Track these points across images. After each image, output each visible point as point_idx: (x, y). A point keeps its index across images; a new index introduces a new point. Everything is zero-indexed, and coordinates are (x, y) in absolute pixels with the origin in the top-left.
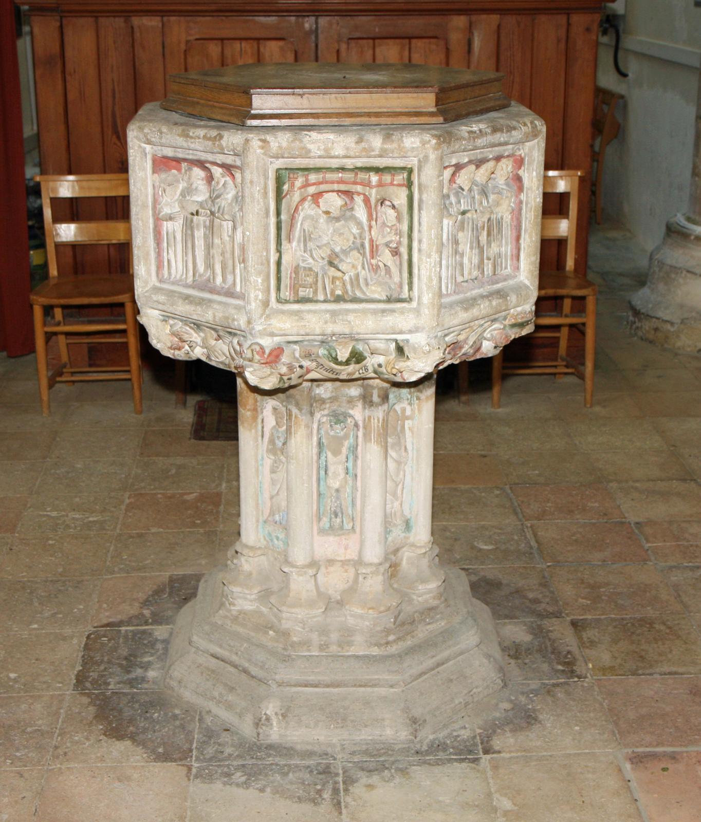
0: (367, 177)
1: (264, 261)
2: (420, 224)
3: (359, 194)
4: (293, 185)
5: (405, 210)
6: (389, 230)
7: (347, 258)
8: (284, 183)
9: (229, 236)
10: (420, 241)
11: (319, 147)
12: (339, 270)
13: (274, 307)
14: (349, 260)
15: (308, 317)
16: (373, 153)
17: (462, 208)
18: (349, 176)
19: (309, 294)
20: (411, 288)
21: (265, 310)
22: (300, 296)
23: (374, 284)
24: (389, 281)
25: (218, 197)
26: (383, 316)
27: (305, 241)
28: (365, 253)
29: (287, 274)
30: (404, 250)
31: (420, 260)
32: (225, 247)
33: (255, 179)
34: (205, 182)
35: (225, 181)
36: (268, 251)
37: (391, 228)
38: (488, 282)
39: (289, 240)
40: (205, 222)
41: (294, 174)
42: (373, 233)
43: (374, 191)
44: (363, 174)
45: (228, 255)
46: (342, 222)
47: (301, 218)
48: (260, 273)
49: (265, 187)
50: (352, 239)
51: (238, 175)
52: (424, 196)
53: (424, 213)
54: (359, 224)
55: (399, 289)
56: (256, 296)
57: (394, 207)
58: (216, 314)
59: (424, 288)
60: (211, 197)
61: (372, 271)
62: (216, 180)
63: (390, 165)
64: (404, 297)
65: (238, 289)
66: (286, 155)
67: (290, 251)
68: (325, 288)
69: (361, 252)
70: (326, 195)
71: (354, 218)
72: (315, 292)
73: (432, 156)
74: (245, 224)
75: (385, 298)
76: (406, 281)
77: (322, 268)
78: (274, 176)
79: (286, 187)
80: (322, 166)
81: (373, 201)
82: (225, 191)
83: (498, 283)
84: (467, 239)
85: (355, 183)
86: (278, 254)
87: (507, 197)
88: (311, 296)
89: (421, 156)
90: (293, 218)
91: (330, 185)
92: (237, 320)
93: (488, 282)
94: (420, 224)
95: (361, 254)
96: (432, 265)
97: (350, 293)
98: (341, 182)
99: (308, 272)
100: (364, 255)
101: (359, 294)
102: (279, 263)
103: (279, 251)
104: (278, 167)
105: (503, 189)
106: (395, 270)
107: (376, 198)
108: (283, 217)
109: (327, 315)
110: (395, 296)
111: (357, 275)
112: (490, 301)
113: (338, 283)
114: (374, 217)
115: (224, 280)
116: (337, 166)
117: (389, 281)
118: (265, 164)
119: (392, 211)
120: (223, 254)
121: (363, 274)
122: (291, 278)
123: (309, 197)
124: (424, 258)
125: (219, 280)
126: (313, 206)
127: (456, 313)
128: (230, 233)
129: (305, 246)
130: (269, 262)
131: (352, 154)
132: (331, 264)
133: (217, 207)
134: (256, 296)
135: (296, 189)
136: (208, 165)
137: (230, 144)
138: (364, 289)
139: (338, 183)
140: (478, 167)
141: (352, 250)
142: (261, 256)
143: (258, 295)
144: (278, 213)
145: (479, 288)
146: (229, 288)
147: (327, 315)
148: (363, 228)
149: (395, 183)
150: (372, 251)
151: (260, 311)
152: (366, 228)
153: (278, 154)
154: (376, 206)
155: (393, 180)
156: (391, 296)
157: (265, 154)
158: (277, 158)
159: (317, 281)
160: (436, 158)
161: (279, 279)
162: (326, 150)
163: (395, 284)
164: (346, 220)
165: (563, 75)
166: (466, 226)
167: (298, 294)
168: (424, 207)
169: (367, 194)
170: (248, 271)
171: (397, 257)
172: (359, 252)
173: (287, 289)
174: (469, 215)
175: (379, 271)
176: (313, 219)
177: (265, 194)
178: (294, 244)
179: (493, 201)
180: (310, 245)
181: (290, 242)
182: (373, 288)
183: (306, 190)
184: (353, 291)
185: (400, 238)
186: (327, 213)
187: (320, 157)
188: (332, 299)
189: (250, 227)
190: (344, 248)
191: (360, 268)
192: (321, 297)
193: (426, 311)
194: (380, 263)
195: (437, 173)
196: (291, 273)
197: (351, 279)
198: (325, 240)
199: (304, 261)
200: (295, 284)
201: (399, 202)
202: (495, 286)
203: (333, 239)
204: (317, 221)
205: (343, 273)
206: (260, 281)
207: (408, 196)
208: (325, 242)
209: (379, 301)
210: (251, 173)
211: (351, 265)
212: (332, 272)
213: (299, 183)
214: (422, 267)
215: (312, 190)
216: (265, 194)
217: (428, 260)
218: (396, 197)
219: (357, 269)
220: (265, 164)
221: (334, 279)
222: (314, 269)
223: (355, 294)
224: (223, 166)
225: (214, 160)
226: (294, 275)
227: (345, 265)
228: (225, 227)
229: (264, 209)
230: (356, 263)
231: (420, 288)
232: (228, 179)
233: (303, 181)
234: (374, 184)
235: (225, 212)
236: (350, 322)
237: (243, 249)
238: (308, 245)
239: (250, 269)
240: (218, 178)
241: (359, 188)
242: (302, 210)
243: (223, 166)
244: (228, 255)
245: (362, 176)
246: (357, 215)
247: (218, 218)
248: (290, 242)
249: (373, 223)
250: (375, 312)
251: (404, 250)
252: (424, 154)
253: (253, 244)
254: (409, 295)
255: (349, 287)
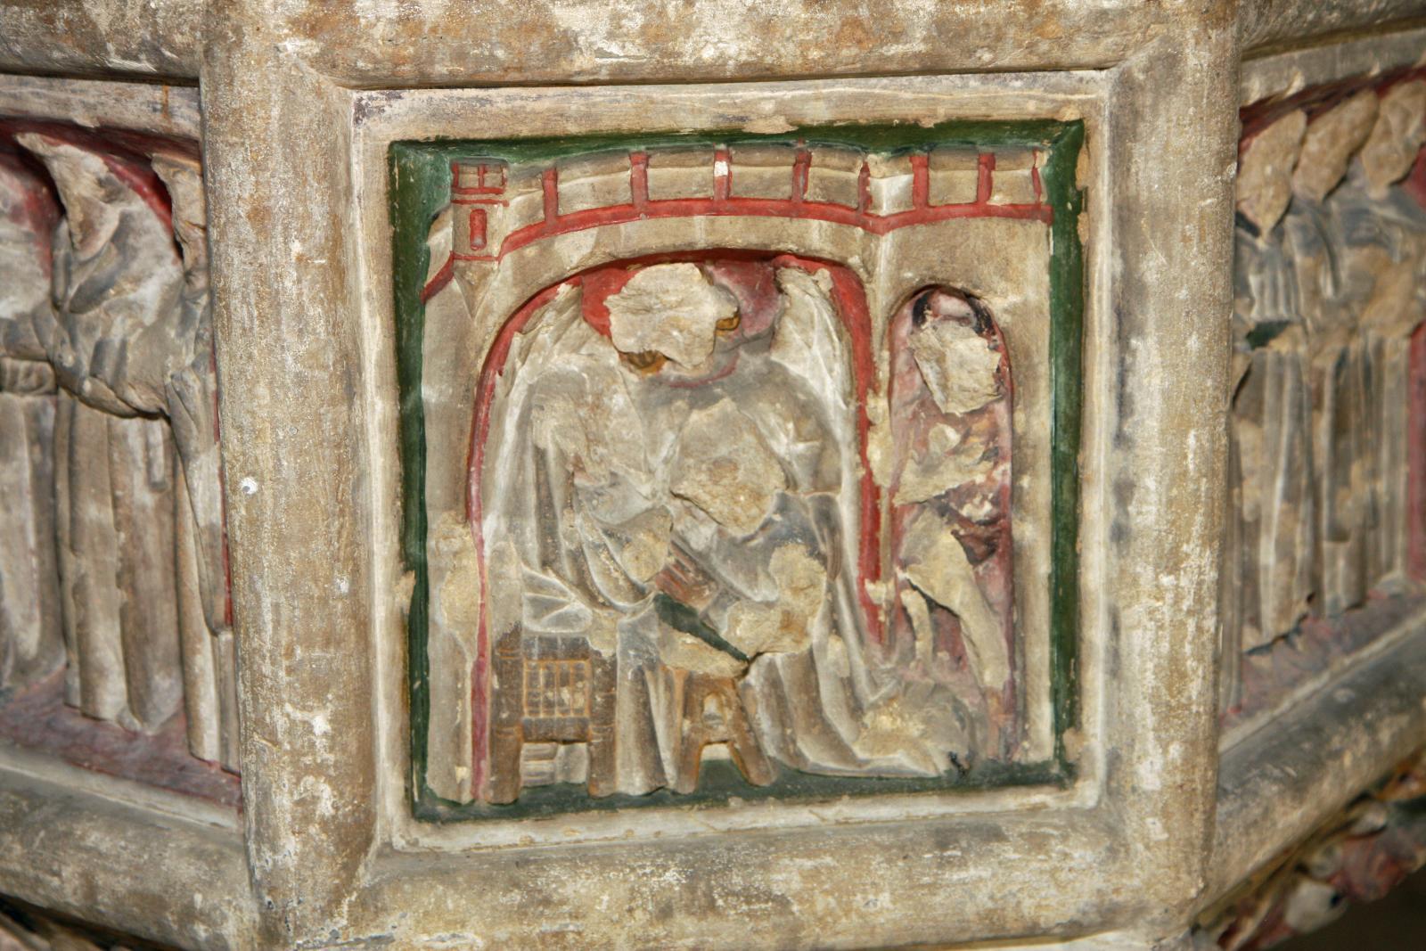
0: (855, 175)
1: (342, 624)
2: (1124, 404)
3: (811, 261)
4: (479, 225)
5: (1039, 336)
6: (953, 436)
7: (753, 579)
8: (433, 219)
9: (154, 486)
10: (1124, 490)
11: (617, 17)
12: (720, 645)
13: (399, 843)
14: (763, 593)
15: (576, 886)
16: (894, 50)
17: (1254, 316)
18: (768, 172)
19: (568, 770)
20: (1068, 715)
21: (349, 869)
22: (524, 779)
23: (890, 699)
24: (948, 678)
25: (92, 295)
26: (944, 863)
27: (545, 507)
28: (838, 551)
29: (457, 677)
30: (1033, 533)
31: (1122, 580)
32: (136, 539)
33: (280, 200)
34: (27, 227)
35: (125, 219)
36: (359, 571)
37: (964, 424)
38: (1338, 638)
39: (467, 509)
40: (35, 416)
41: (483, 170)
42: (875, 453)
43: (886, 246)
44: (834, 160)
45: (154, 579)
46: (726, 405)
47: (518, 395)
48: (316, 689)
49: (336, 242)
50: (774, 483)
51: (185, 187)
52: (1152, 267)
53: (1147, 350)
54: (806, 412)
55: (1005, 721)
56: (306, 804)
57: (984, 323)
58: (101, 879)
59: (1145, 714)
60: (56, 304)
61: (869, 637)
62: (76, 214)
63: (975, 111)
64: (1034, 757)
65: (210, 747)
66: (441, 69)
67: (471, 562)
68: (648, 738)
69: (824, 548)
70: (642, 278)
71: (779, 383)
72: (604, 760)
73: (1197, 59)
74: (231, 434)
75: (942, 766)
76: (1042, 682)
77: (635, 636)
78: (380, 183)
79: (441, 240)
80: (626, 126)
81: (880, 296)
82: (124, 265)
83: (1372, 637)
84: (1275, 454)
85: (796, 208)
86: (409, 582)
87: (1406, 258)
88: (580, 777)
89: (1137, 61)
90: (480, 396)
91: (673, 222)
92: (205, 917)
93: (1338, 638)
94: (1124, 404)
95: (822, 558)
96: (1186, 604)
97: (771, 750)
98: (727, 202)
99: (567, 665)
100: (834, 564)
101: (815, 755)
102: (415, 625)
103: (414, 562)
104: (397, 134)
105: (1388, 222)
106: (982, 630)
107: (897, 281)
108: (431, 392)
109: (671, 876)
110: (991, 750)
111: (809, 664)
112: (1371, 728)
113: (711, 706)
114: (883, 373)
115: (138, 699)
116: (704, 123)
117: (948, 678)
118: (328, 118)
119: (979, 343)
120: (127, 575)
121: (834, 654)
122: (478, 692)
123: (564, 289)
124: (1145, 572)
125: (112, 697)
126: (581, 328)
127: (1267, 812)
128: (160, 472)
129: (548, 531)
130: (363, 626)
131: (787, 54)
132: (675, 612)
133: (86, 346)
134: (306, 804)
135: (495, 248)
136: (30, 140)
137: (133, 13)
138: (843, 728)
139: (712, 207)
140: (1312, 117)
141: (776, 542)
142: (324, 601)
143: (315, 799)
144: (406, 375)
145: (1316, 672)
146: (162, 740)
147: (671, 876)
148: (824, 432)
149: (997, 200)
150: (870, 542)
151: (326, 875)
152: (842, 431)
153: (397, 61)
154: (892, 321)
155: (986, 186)
156: (972, 755)
157: (325, 62)
158: (394, 86)
159: (611, 702)
160: (1215, 66)
161: (416, 702)
162: (655, 35)
163: (985, 693)
164: (743, 393)
165: (646, 89)
166: (1268, 395)
167: (515, 772)
168: (1151, 316)
169: (854, 261)
170: (257, 680)
171: (994, 569)
172: (814, 553)
173: (458, 748)
174: (1280, 346)
175: (903, 634)
176: (578, 396)
177: (337, 275)
178: (492, 524)
179: (1355, 276)
180: (576, 527)
181: (468, 516)
182: (886, 722)
183: (545, 251)
184: (786, 742)
185: (1017, 473)
186: (644, 361)
187: (621, 78)
188: (688, 788)
189: (264, 453)
190: (738, 533)
191: (816, 628)
192: (633, 781)
193: (1156, 829)
194: (913, 603)
195: (1216, 144)
196: (479, 668)
197: (774, 683)
198: (642, 492)
199: (542, 607)
200: (499, 726)
201: (1014, 298)
202: (1366, 653)
203: (684, 488)
204: (596, 407)
205: (738, 656)
206: (321, 723)
207: (1054, 266)
208: (639, 505)
209: (917, 786)
210: (257, 168)
211: (775, 616)
212: (685, 653)
213: (506, 218)
214: (1134, 614)
215: (576, 249)
216: (337, 275)
217: (1166, 580)
218: (1005, 271)
219: (804, 633)
220: (328, 118)
221: (694, 690)
222: (594, 644)
223: (798, 756)
224: (105, 139)
225: (57, 113)
226: (494, 682)
227: (747, 618)
228: (135, 442)
229: (330, 357)
230: (799, 604)
231: (1118, 717)
232: (139, 206)
233: (531, 206)
234: (885, 210)
235: (130, 371)
236: (782, 903)
237: (225, 552)
238: (562, 527)
239: (267, 669)
240: (87, 203)
241: (816, 234)
242: (525, 353)
243: (105, 139)
244: (154, 579)
245: (828, 169)
246: (795, 369)
247: (94, 403)
248: (468, 516)
249: (877, 405)
250: (901, 843)
251: (1033, 533)
252: (1152, 48)
253: (281, 540)
254: (1060, 749)
255: (764, 721)
